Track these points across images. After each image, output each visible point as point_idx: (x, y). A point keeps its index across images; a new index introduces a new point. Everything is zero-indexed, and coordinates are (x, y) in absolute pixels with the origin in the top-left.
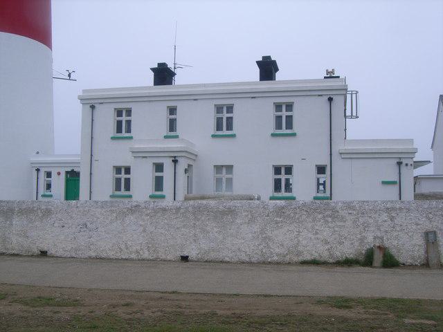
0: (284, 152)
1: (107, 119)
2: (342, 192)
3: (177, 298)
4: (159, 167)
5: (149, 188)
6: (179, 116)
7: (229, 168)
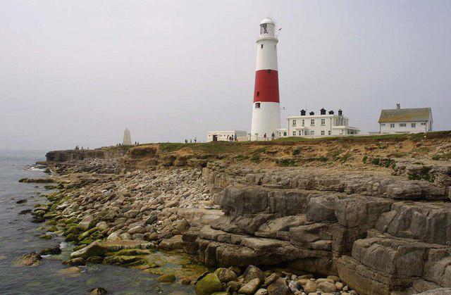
1: (291, 122)
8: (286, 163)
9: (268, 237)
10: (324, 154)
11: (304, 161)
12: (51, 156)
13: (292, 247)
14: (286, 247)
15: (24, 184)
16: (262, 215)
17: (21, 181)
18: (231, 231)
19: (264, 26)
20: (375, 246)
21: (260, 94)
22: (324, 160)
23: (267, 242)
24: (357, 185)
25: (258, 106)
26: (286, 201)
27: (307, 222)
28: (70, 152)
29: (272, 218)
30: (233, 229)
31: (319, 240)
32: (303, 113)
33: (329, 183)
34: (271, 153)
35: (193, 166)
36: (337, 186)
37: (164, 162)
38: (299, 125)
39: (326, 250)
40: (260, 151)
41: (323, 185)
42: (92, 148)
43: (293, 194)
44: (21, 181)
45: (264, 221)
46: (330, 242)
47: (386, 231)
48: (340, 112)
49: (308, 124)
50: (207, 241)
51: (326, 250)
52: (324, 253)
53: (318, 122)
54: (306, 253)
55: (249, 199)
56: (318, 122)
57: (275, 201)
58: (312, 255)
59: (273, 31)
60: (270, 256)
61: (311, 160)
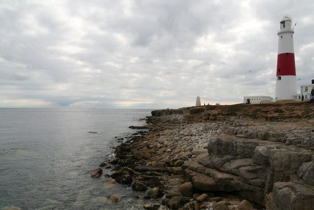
1: (304, 89)
8: (272, 119)
9: (227, 172)
10: (300, 113)
11: (285, 118)
12: (154, 113)
13: (239, 182)
14: (236, 180)
15: (91, 133)
16: (229, 157)
17: (96, 133)
18: (207, 166)
19: (283, 23)
20: (285, 189)
21: (281, 71)
22: (299, 117)
23: (225, 176)
24: (294, 138)
25: (280, 78)
26: (244, 147)
27: (252, 164)
28: (164, 111)
29: (234, 159)
30: (208, 164)
31: (257, 178)
33: (279, 135)
34: (264, 112)
35: (219, 120)
36: (283, 139)
37: (204, 118)
39: (260, 186)
40: (257, 110)
41: (274, 137)
42: (176, 108)
43: (249, 143)
44: (130, 127)
45: (228, 161)
46: (264, 180)
47: (301, 178)
50: (191, 171)
51: (260, 186)
52: (258, 188)
54: (246, 186)
55: (221, 144)
57: (236, 147)
58: (250, 189)
59: (290, 26)
60: (224, 186)
61: (291, 117)
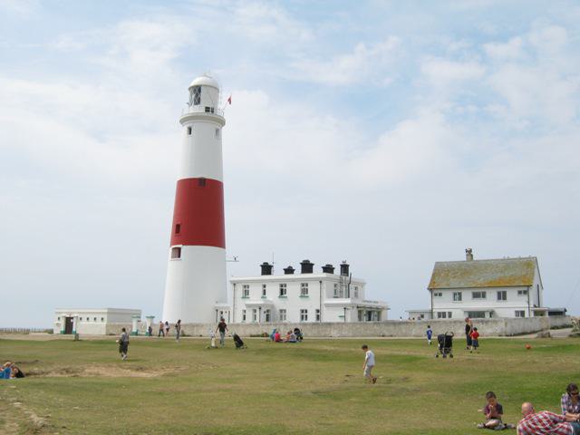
0: (304, 304)
1: (240, 290)
2: (326, 318)
3: (529, 357)
4: (255, 311)
5: (241, 318)
6: (267, 288)
7: (285, 311)
32: (267, 269)
38: (255, 298)
48: (345, 268)
49: (273, 292)
53: (294, 290)
56: (294, 290)
